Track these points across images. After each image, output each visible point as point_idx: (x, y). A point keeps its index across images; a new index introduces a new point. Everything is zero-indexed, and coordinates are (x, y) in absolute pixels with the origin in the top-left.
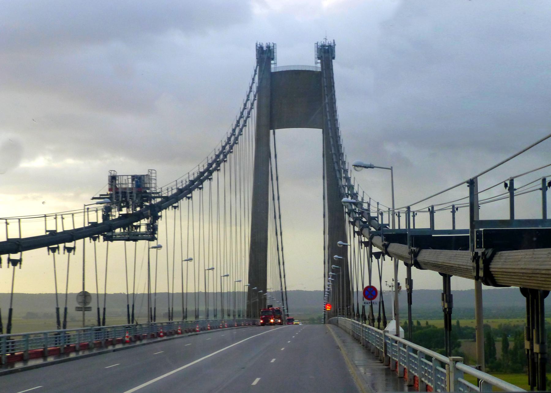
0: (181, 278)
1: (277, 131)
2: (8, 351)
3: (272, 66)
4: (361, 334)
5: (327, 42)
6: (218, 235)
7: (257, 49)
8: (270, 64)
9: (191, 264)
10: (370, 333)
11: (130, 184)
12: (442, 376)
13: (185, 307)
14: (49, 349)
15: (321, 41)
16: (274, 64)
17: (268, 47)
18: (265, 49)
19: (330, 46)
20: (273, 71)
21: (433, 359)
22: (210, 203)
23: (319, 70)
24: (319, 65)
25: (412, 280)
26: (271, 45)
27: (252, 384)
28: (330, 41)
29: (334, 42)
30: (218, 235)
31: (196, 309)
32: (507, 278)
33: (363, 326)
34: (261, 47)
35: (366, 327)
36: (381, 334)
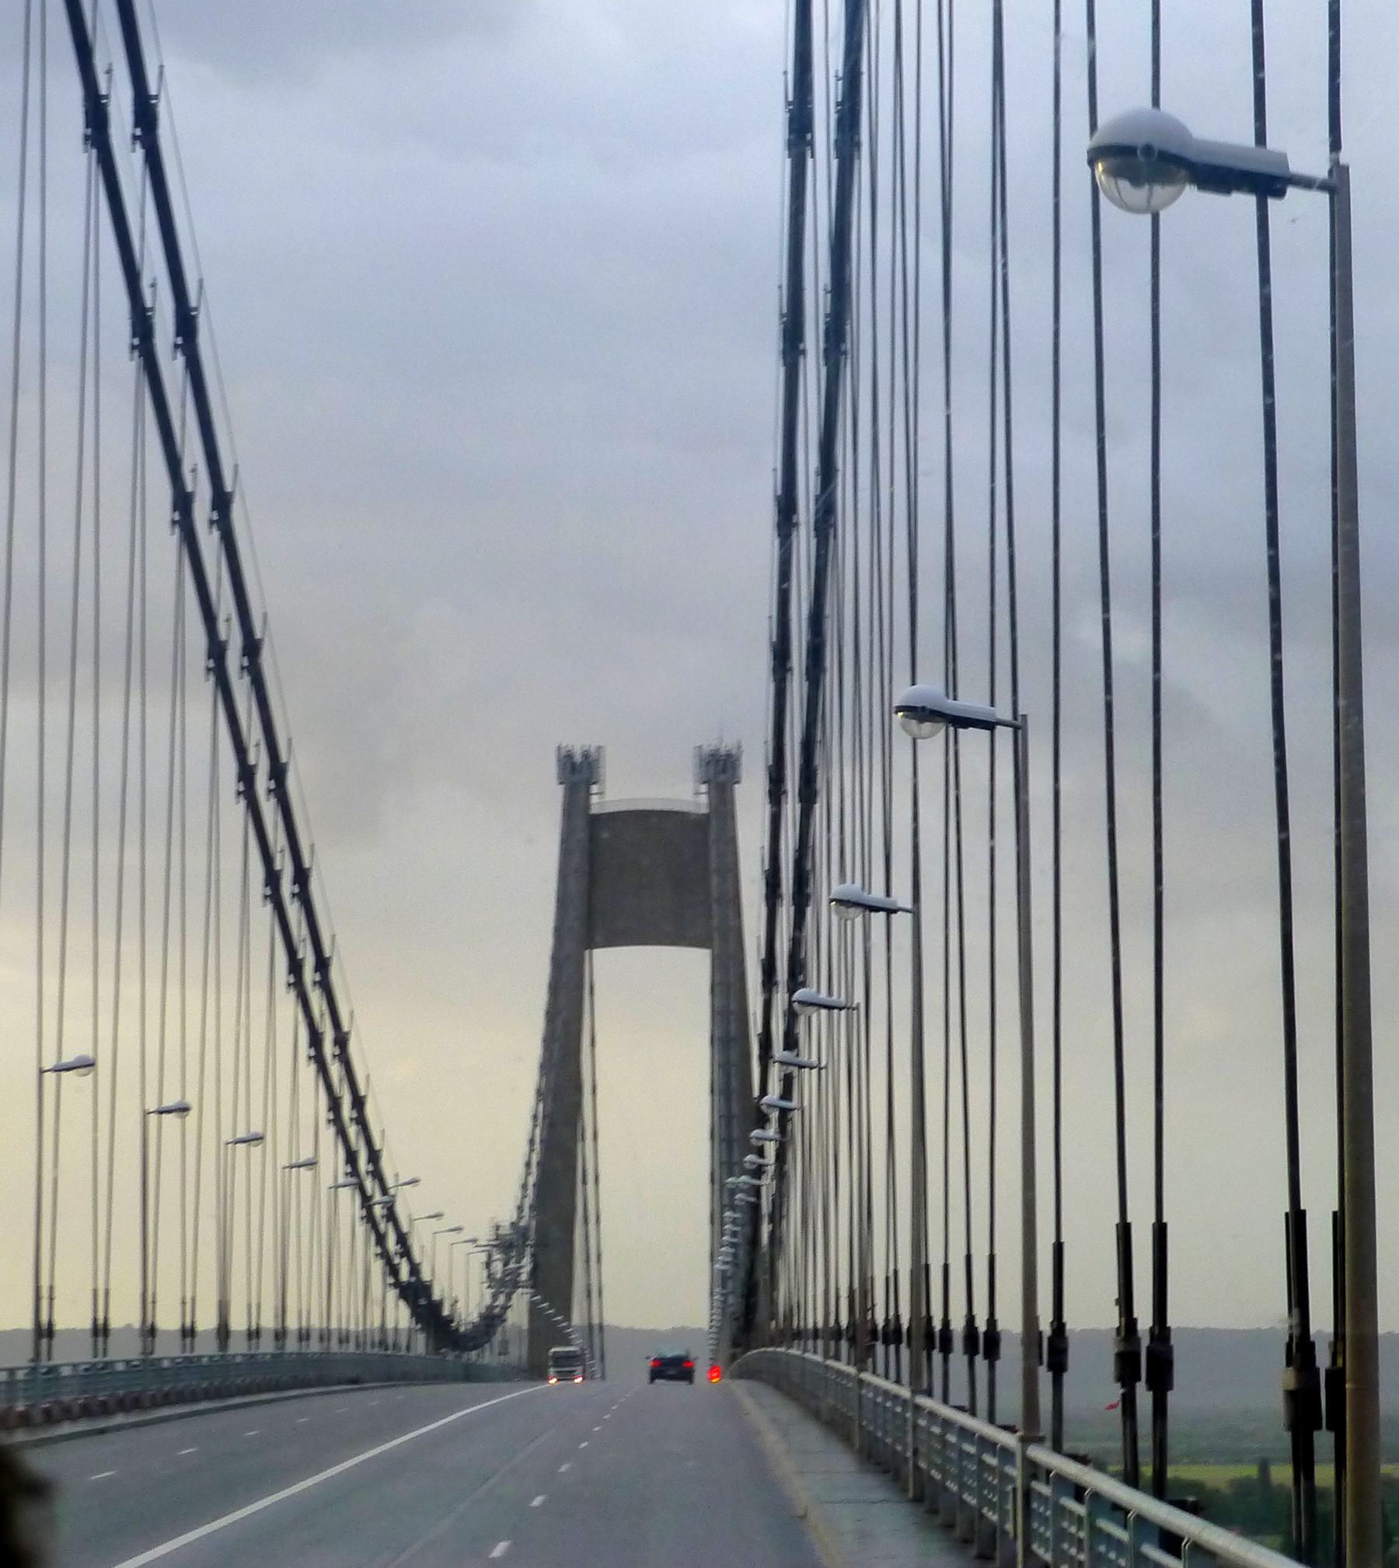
0: (60, 1151)
1: (596, 952)
2: (46, 1396)
3: (594, 799)
4: (905, 1445)
5: (724, 744)
6: (178, 732)
7: (559, 761)
8: (589, 794)
9: (256, 1151)
10: (952, 1445)
11: (390, 1186)
12: (416, 1281)
13: (44, 1319)
14: (100, 1399)
15: (709, 743)
16: (601, 793)
17: (586, 755)
18: (578, 758)
19: (729, 755)
20: (595, 810)
21: (1185, 1545)
22: (133, 515)
23: (704, 810)
24: (704, 799)
25: (1304, 1211)
26: (593, 749)
27: (490, 1557)
28: (727, 744)
29: (739, 747)
30: (178, 732)
31: (95, 1320)
32: (799, 1313)
33: (917, 1408)
34: (569, 756)
35: (932, 1415)
36: (1006, 1454)
